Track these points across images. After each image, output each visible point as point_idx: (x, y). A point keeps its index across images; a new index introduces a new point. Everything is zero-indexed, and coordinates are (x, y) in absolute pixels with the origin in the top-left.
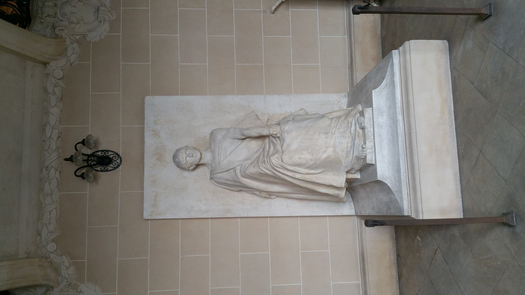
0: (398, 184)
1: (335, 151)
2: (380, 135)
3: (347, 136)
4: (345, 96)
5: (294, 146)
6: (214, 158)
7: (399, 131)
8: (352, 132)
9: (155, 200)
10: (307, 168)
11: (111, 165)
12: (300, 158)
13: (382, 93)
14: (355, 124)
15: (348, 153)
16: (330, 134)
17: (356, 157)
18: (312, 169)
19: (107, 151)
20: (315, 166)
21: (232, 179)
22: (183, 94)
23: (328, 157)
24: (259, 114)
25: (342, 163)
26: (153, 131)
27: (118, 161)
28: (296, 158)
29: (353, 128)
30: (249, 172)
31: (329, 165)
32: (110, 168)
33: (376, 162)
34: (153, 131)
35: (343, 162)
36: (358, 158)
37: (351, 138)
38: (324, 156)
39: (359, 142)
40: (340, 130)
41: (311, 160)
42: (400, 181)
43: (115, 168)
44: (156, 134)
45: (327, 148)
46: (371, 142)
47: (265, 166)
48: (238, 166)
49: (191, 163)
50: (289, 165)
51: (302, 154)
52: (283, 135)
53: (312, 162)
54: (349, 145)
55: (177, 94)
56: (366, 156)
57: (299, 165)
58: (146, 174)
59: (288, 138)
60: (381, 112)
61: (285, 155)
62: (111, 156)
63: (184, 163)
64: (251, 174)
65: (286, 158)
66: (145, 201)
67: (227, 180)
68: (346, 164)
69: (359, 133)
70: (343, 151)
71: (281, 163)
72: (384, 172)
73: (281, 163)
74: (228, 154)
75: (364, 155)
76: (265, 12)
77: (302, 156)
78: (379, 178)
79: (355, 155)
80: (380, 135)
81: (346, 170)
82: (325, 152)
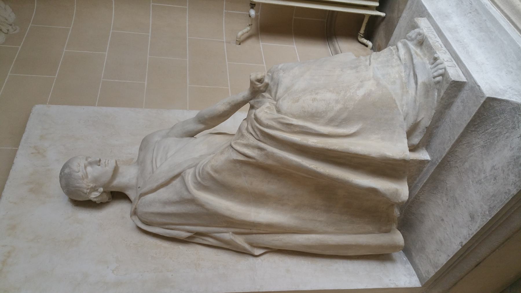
1: (378, 84)
2: (458, 41)
8: (402, 57)
10: (331, 122)
12: (314, 100)
15: (404, 86)
17: (424, 84)
18: (339, 125)
20: (344, 115)
21: (175, 198)
22: (101, 105)
23: (368, 95)
25: (397, 107)
28: (308, 102)
31: (372, 113)
33: (466, 73)
35: (398, 103)
36: (428, 88)
38: (361, 93)
39: (421, 59)
41: (337, 102)
44: (39, 153)
47: (245, 142)
48: (190, 167)
49: (95, 180)
50: (294, 116)
51: (317, 94)
52: (275, 76)
53: (338, 107)
55: (94, 105)
57: (313, 116)
59: (286, 79)
60: (446, 16)
63: (80, 174)
64: (216, 171)
65: (286, 104)
68: (405, 108)
70: (394, 83)
71: (276, 115)
73: (276, 115)
75: (441, 71)
77: (318, 97)
78: (487, 96)
79: (420, 81)
80: (458, 41)
82: (359, 88)
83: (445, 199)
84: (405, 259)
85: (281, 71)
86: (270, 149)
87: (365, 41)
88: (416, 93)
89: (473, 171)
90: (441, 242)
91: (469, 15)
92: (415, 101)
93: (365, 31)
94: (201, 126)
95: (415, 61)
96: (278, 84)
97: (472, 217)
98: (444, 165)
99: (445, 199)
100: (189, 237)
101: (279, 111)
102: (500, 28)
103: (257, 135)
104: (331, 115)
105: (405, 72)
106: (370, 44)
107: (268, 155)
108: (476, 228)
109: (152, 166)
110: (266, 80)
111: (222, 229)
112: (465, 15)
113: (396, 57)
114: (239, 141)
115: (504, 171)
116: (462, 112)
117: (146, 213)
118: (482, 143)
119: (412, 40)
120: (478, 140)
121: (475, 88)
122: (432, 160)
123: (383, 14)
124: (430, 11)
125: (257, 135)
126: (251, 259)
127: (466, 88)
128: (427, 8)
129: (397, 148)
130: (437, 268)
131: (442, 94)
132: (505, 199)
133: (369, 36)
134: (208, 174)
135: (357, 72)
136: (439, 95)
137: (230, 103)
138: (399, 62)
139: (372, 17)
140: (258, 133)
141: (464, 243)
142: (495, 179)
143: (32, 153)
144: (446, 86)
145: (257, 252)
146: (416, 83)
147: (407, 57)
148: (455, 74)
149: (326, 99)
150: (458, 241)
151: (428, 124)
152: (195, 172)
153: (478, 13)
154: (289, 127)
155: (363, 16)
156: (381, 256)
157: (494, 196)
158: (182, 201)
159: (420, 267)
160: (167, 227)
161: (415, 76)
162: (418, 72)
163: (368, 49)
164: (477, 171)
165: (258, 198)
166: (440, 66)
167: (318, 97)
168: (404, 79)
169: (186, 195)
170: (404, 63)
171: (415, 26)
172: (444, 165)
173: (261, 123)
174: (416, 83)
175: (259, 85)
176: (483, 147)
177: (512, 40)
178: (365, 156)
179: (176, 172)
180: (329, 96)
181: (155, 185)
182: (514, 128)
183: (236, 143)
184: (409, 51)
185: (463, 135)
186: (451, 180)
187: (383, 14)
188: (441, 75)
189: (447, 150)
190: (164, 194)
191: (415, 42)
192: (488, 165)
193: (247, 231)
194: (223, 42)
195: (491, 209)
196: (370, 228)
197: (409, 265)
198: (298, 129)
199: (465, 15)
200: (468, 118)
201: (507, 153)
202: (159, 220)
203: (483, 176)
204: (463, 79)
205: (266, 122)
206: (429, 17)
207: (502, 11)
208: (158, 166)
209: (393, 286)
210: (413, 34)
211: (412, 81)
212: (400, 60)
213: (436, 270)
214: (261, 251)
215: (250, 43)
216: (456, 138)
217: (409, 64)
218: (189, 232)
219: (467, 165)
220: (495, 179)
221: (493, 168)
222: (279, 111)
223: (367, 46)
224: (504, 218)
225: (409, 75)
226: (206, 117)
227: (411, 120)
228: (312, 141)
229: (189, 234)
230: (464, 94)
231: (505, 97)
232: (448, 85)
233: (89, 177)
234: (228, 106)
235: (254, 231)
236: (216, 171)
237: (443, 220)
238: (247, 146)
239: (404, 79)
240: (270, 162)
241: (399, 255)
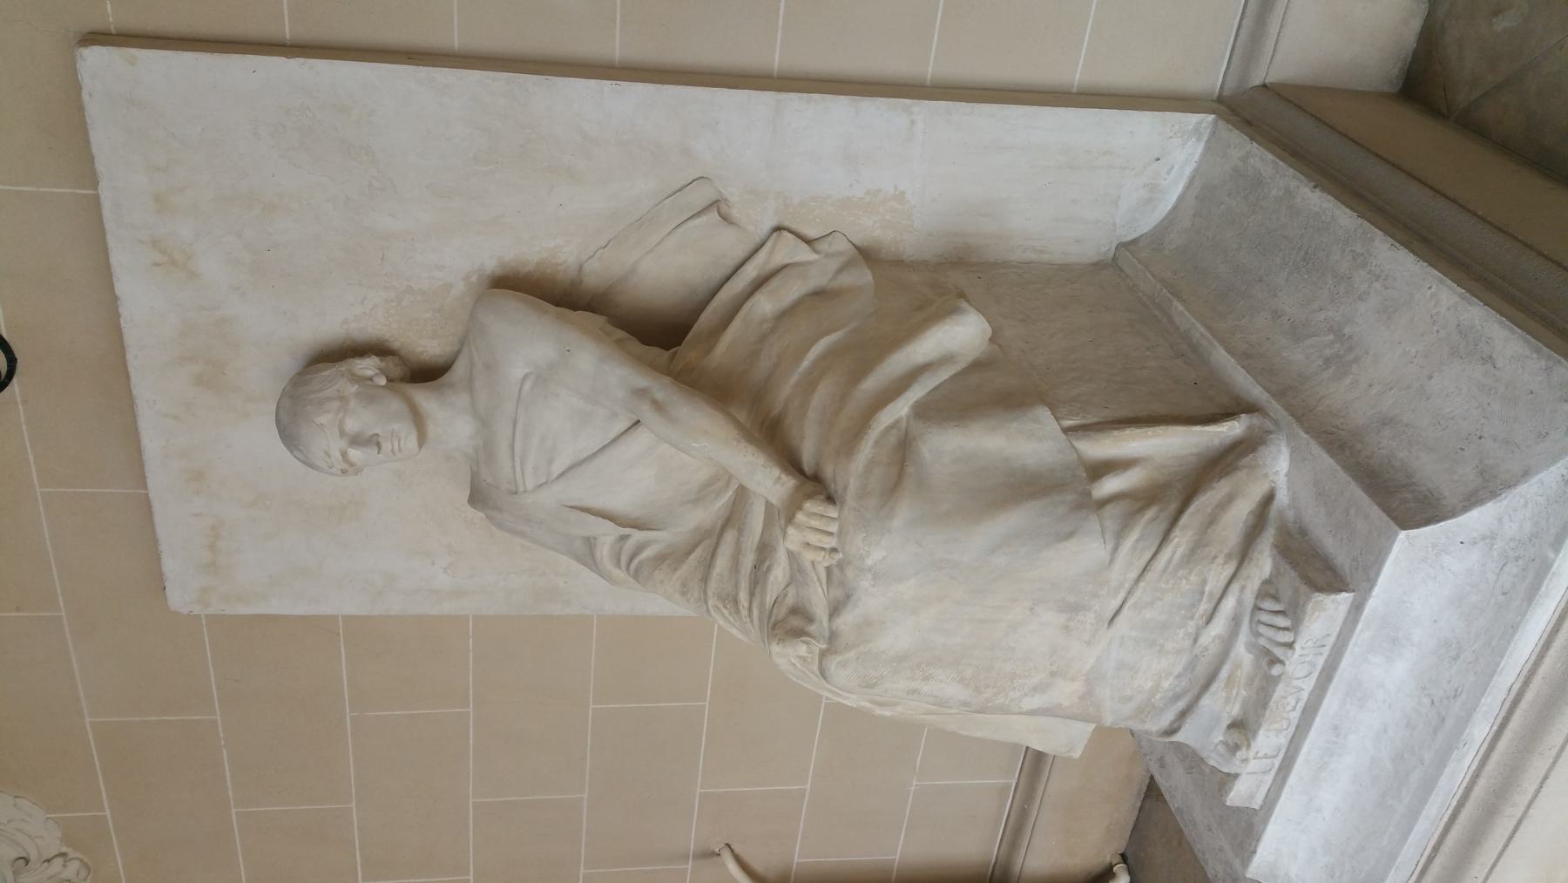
2: (1336, 728)
3: (1169, 646)
4: (1197, 130)
5: (897, 638)
7: (1443, 782)
8: (1205, 640)
13: (1447, 559)
14: (1236, 621)
16: (1090, 618)
24: (733, 194)
26: (155, 243)
29: (1219, 627)
34: (155, 243)
37: (1184, 659)
40: (1148, 614)
44: (173, 262)
45: (1053, 674)
46: (1279, 731)
51: (926, 679)
52: (850, 573)
54: (1166, 684)
56: (1236, 776)
58: (151, 444)
66: (164, 547)
69: (1237, 666)
74: (557, 468)
80: (1336, 728)
81: (1129, 855)
82: (1036, 689)
85: (870, 576)
91: (1426, 701)
95: (1206, 701)
96: (848, 597)
102: (1413, 815)
105: (1179, 676)
109: (513, 467)
112: (1424, 689)
113: (1191, 627)
128: (1377, 590)
135: (1066, 628)
138: (1188, 643)
143: (156, 264)
147: (1214, 649)
153: (1435, 732)
167: (926, 688)
168: (1158, 696)
170: (1197, 651)
177: (1393, 857)
199: (1424, 689)
207: (1476, 776)
212: (1195, 641)
217: (1201, 670)
225: (1177, 697)
239: (1158, 696)
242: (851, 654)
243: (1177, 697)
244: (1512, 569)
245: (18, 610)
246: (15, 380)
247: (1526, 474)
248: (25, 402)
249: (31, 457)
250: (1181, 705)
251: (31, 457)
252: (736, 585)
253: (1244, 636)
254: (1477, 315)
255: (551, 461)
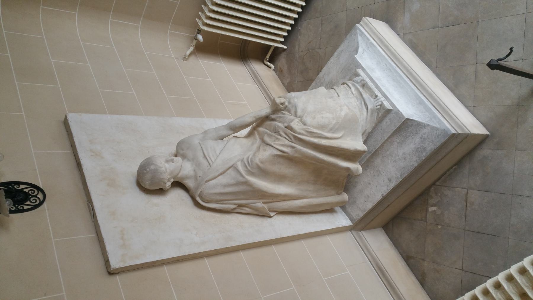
0: (427, 114)
6: (198, 165)
8: (354, 92)
9: (122, 238)
11: (28, 203)
14: (354, 85)
17: (371, 109)
19: (18, 183)
20: (337, 127)
21: (233, 182)
23: (346, 115)
26: (91, 150)
27: (40, 196)
29: (353, 89)
30: (259, 159)
31: (346, 125)
32: (26, 207)
33: (392, 104)
34: (91, 150)
38: (343, 114)
41: (333, 119)
42: (428, 110)
43: (35, 207)
44: (97, 155)
47: (281, 143)
48: (238, 161)
52: (292, 101)
53: (334, 122)
57: (322, 127)
61: (306, 117)
62: (27, 190)
64: (262, 162)
65: (308, 120)
67: (225, 186)
72: (408, 109)
74: (218, 152)
75: (380, 103)
76: (177, 59)
79: (370, 107)
83: (372, 172)
84: (341, 210)
86: (299, 147)
87: (269, 64)
88: (367, 114)
89: (391, 156)
90: (368, 196)
92: (367, 119)
93: (270, 57)
94: (232, 132)
96: (296, 107)
97: (390, 180)
98: (375, 154)
99: (372, 172)
100: (235, 209)
101: (305, 124)
103: (291, 139)
104: (331, 126)
106: (272, 66)
107: (297, 151)
108: (392, 185)
110: (287, 104)
111: (256, 201)
114: (277, 142)
115: (410, 155)
116: (389, 126)
117: (211, 194)
118: (398, 141)
119: (357, 83)
120: (397, 140)
121: (398, 113)
122: (368, 151)
123: (285, 47)
124: (363, 66)
125: (291, 139)
126: (269, 219)
127: (393, 112)
129: (357, 144)
130: (365, 211)
131: (380, 114)
132: (411, 169)
133: (271, 60)
134: (257, 164)
136: (378, 115)
137: (255, 117)
139: (276, 48)
140: (292, 137)
141: (385, 194)
142: (405, 159)
144: (383, 111)
145: (272, 214)
146: (367, 109)
148: (387, 105)
149: (326, 118)
150: (381, 194)
151: (370, 131)
152: (245, 164)
154: (311, 134)
155: (270, 46)
156: (329, 210)
157: (404, 168)
158: (238, 184)
159: (352, 214)
160: (222, 202)
161: (366, 104)
162: (367, 102)
163: (271, 70)
164: (394, 156)
165: (280, 178)
166: (379, 100)
169: (241, 179)
171: (357, 75)
172: (375, 154)
173: (295, 131)
174: (367, 109)
175: (281, 106)
176: (399, 143)
178: (347, 149)
179: (231, 164)
180: (329, 115)
181: (217, 174)
182: (416, 134)
183: (274, 144)
184: (357, 89)
185: (390, 137)
186: (378, 161)
187: (285, 47)
188: (380, 105)
189: (379, 145)
190: (222, 180)
191: (360, 84)
192: (401, 152)
193: (268, 201)
194: (173, 58)
195: (402, 175)
196: (333, 192)
197: (344, 214)
198: (316, 135)
200: (394, 129)
201: (412, 146)
202: (219, 198)
203: (397, 158)
204: (391, 108)
205: (299, 131)
206: (363, 69)
208: (213, 160)
209: (341, 226)
210: (358, 79)
211: (364, 108)
213: (364, 213)
214: (274, 214)
215: (192, 59)
216: (386, 138)
217: (359, 97)
218: (235, 204)
219: (388, 153)
220: (405, 159)
221: (404, 153)
222: (305, 124)
223: (270, 68)
224: (226, 202)
225: (361, 103)
226: (237, 126)
227: (364, 129)
228: (324, 142)
229: (235, 206)
230: (391, 116)
231: (413, 119)
232: (384, 111)
233: (168, 171)
234: (254, 119)
235: (275, 200)
236: (262, 162)
237: (370, 184)
238: (283, 145)
240: (296, 155)
241: (338, 209)
242: (306, 114)
243: (361, 103)
244: (370, 49)
245: (45, 295)
246: (45, 203)
247: (358, 42)
248: (48, 209)
249: (50, 228)
250: (363, 103)
251: (50, 228)
252: (274, 136)
253: (357, 85)
254: (336, 54)
255: (215, 152)
